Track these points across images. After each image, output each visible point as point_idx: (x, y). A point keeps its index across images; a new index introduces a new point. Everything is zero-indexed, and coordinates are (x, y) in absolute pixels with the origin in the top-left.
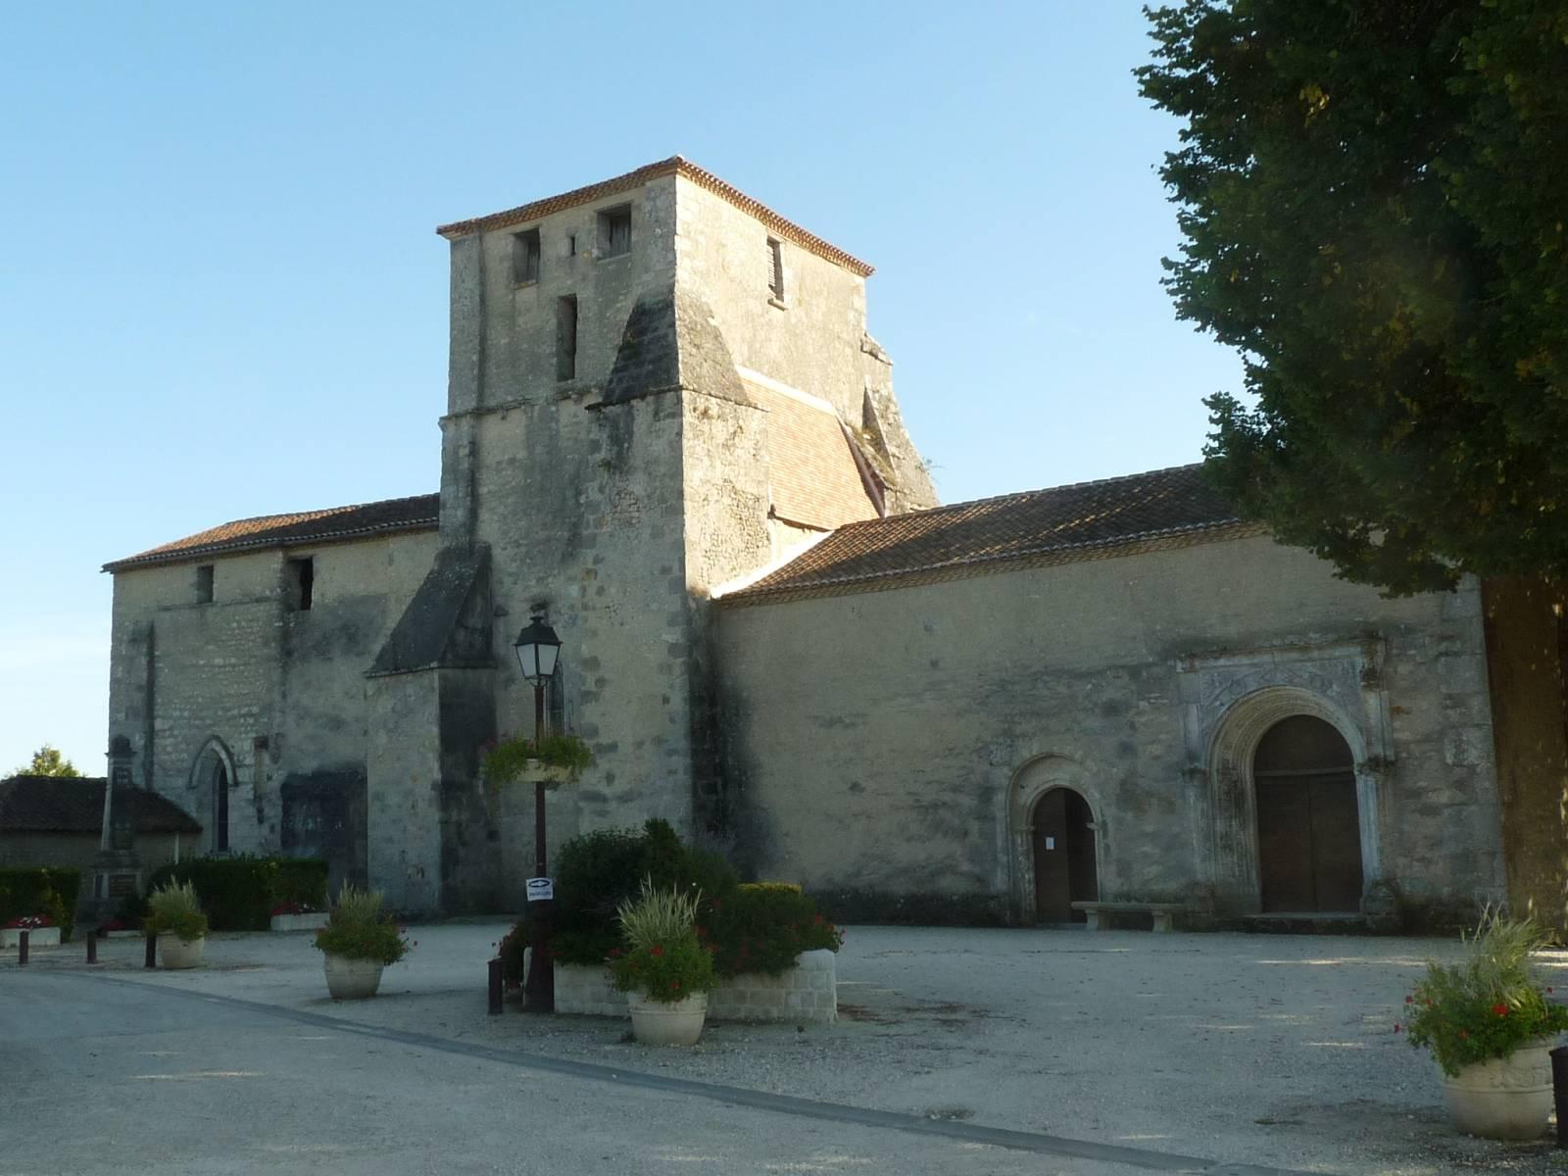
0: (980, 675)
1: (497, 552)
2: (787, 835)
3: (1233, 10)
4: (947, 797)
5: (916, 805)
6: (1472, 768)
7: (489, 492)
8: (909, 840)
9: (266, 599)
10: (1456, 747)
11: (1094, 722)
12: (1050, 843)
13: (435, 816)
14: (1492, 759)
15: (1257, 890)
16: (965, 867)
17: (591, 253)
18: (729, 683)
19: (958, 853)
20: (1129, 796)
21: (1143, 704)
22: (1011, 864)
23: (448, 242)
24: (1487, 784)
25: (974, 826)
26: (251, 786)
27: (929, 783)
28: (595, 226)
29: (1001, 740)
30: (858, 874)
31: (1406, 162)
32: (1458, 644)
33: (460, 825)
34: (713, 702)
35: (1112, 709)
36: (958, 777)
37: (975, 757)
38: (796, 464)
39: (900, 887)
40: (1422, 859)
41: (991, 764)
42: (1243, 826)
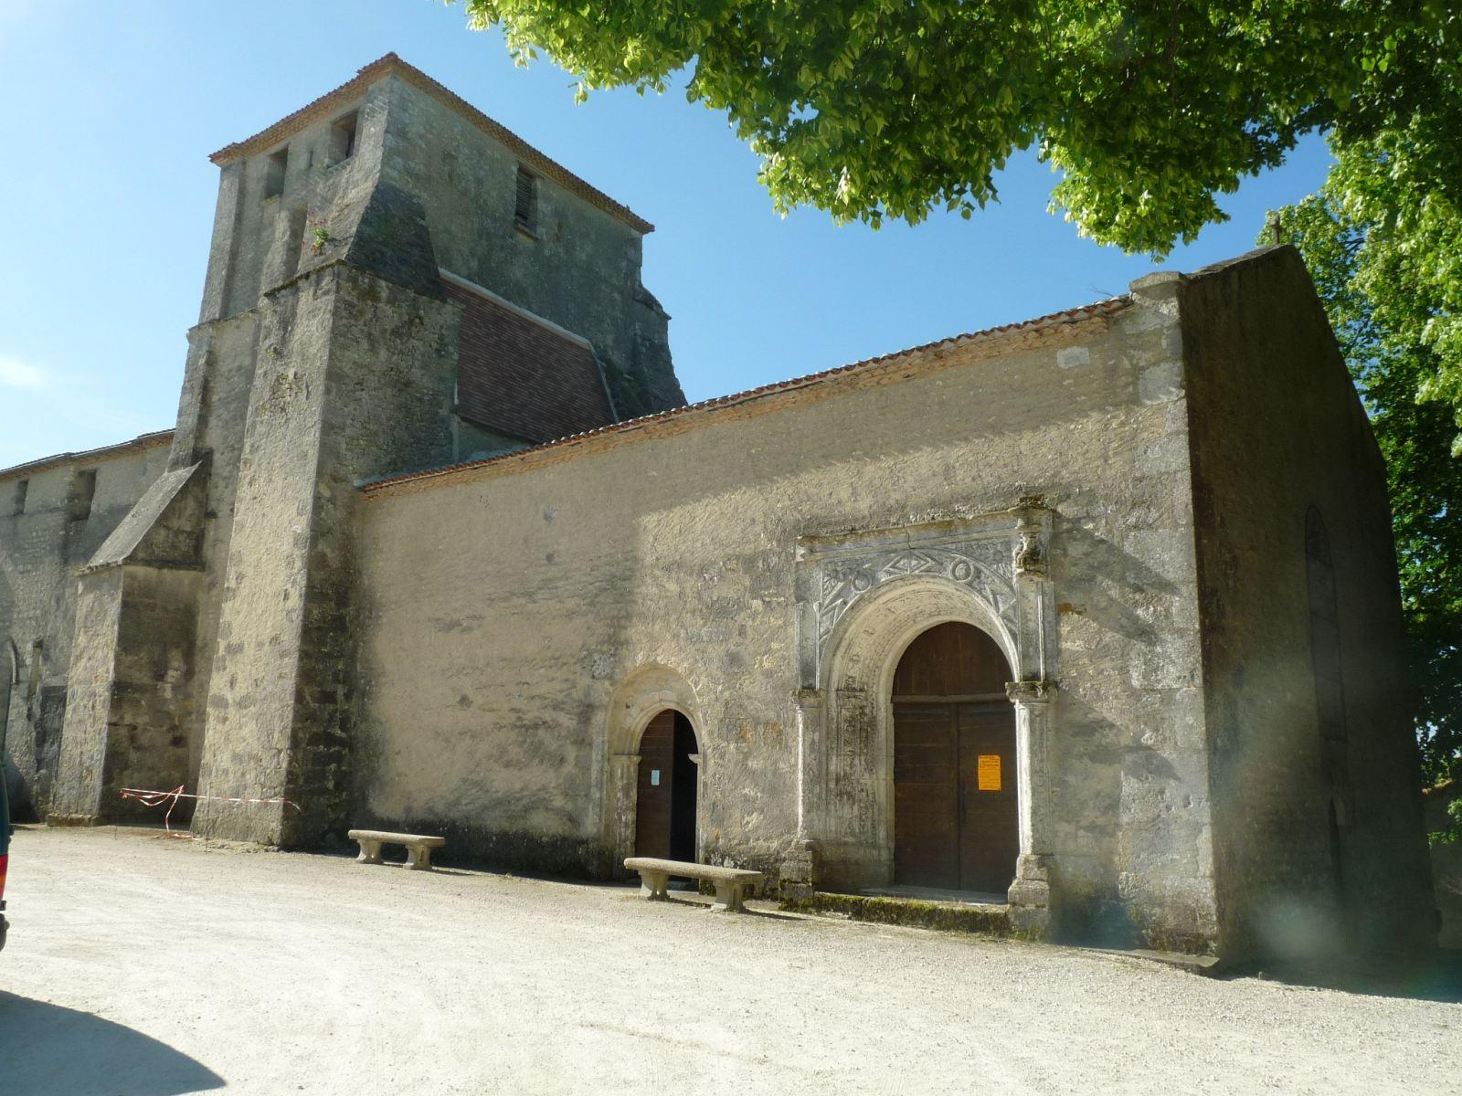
0: (592, 570)
1: (217, 456)
2: (398, 753)
3: (1353, 386)
4: (548, 715)
5: (519, 723)
6: (1168, 696)
7: (219, 399)
8: (508, 765)
9: (57, 509)
10: (1145, 664)
11: (698, 626)
12: (655, 777)
13: (103, 713)
14: (1199, 681)
15: (885, 855)
16: (558, 802)
17: (323, 162)
18: (367, 582)
19: (553, 785)
20: (733, 725)
21: (757, 604)
22: (605, 802)
23: (220, 169)
24: (1190, 720)
25: (571, 753)
26: (27, 685)
27: (533, 698)
28: (329, 137)
29: (605, 648)
30: (457, 802)
31: (1182, 27)
32: (1154, 514)
33: (135, 728)
34: (342, 601)
35: (721, 611)
36: (561, 692)
37: (578, 668)
38: (511, 376)
39: (495, 822)
40: (1092, 828)
41: (593, 677)
42: (871, 767)
